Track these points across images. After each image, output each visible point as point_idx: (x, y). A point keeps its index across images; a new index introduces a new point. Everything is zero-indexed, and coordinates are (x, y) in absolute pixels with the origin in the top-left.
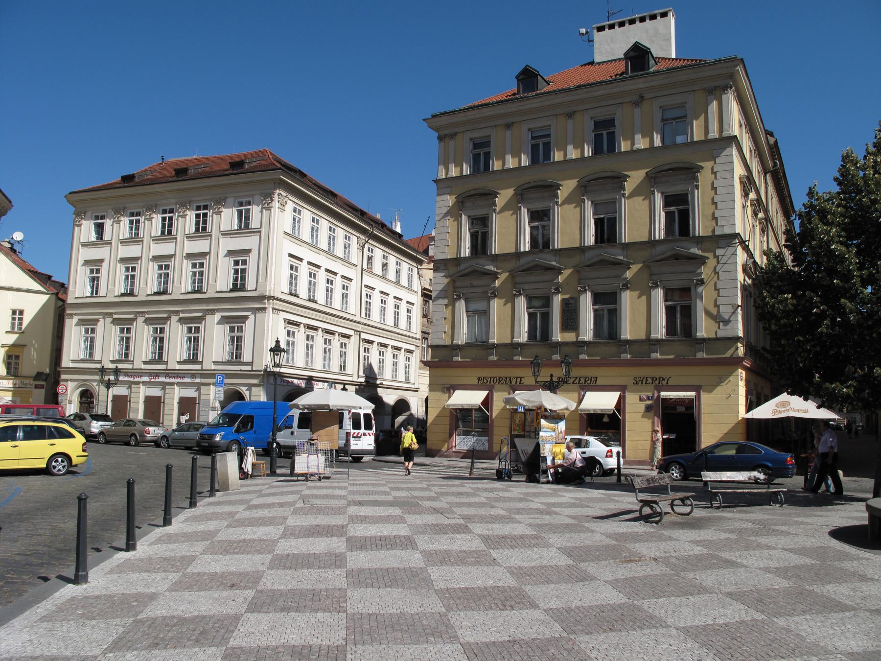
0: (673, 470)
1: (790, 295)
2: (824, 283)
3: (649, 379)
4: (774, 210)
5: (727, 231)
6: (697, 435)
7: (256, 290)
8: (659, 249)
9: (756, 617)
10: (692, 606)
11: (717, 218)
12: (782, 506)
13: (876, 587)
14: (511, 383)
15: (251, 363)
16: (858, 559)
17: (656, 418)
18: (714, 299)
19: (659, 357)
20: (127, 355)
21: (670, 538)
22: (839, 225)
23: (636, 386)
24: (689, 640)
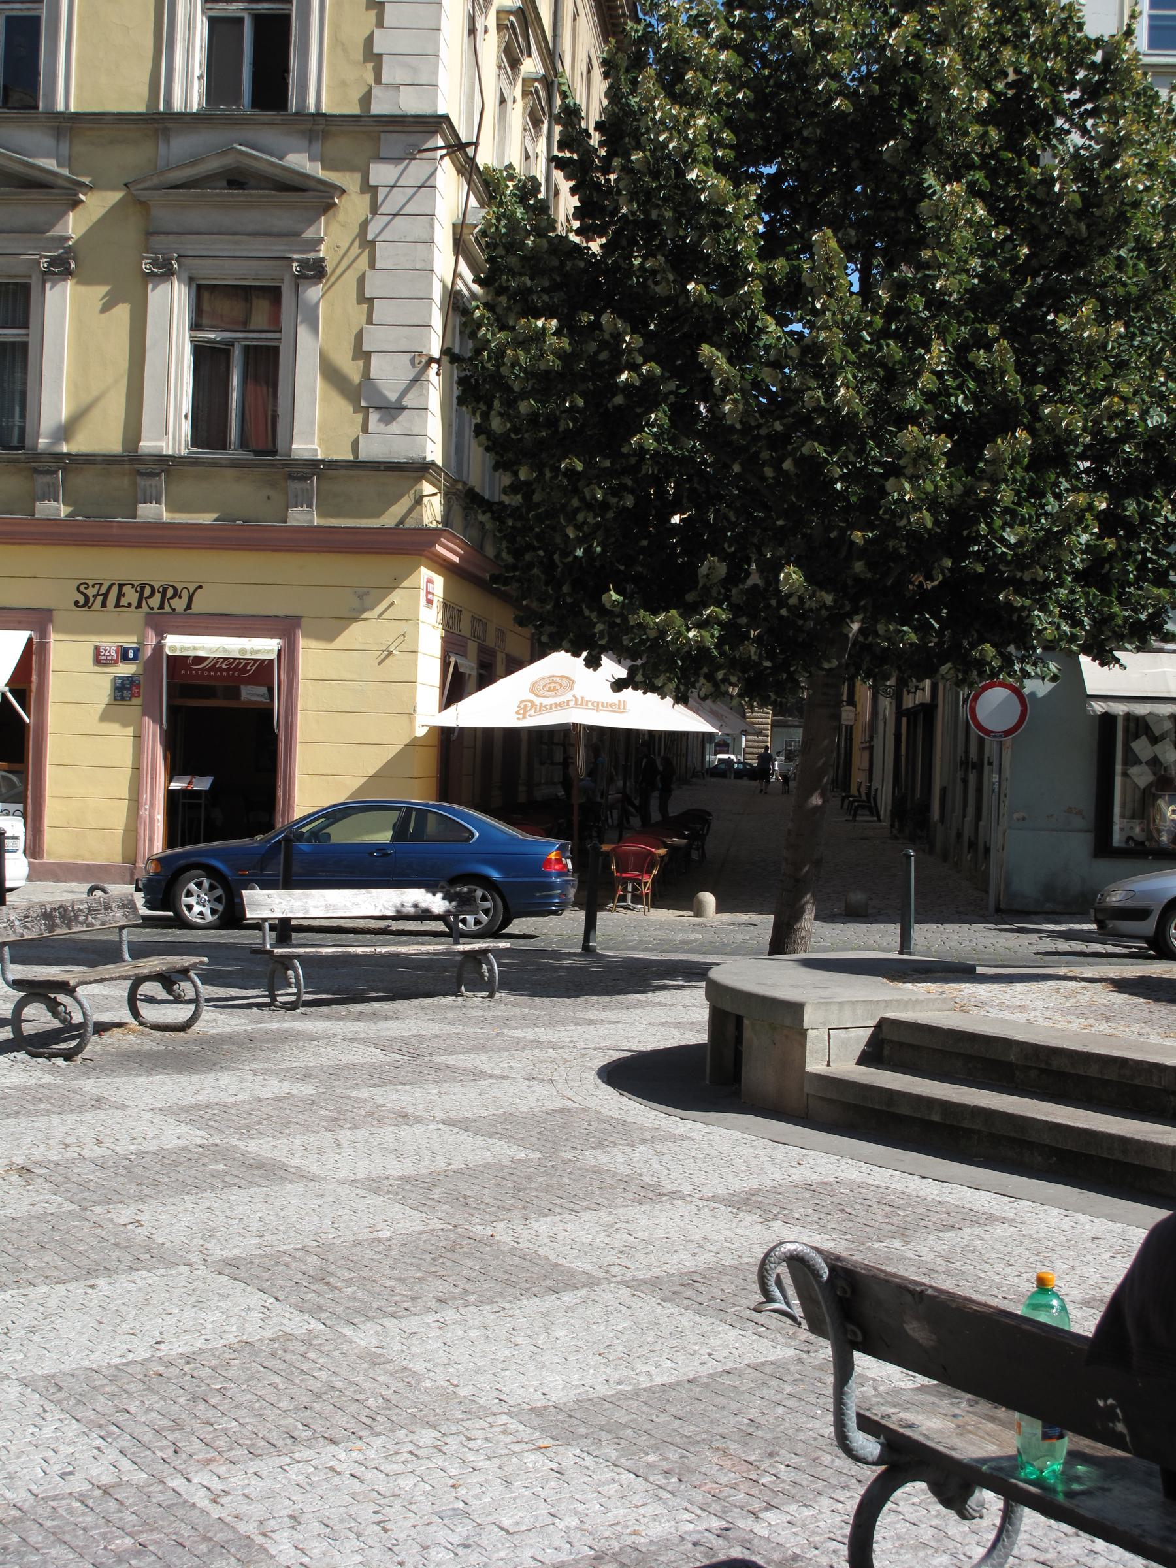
0: (189, 894)
1: (554, 322)
2: (658, 289)
3: (126, 589)
4: (582, 57)
5: (410, 104)
6: (280, 782)
8: (182, 145)
9: (290, 1327)
10: (97, 1310)
11: (380, 55)
12: (491, 996)
13: (676, 1216)
16: (657, 1138)
17: (149, 724)
18: (355, 331)
19: (166, 517)
21: (99, 1102)
22: (717, 105)
23: (83, 614)
24: (55, 1414)
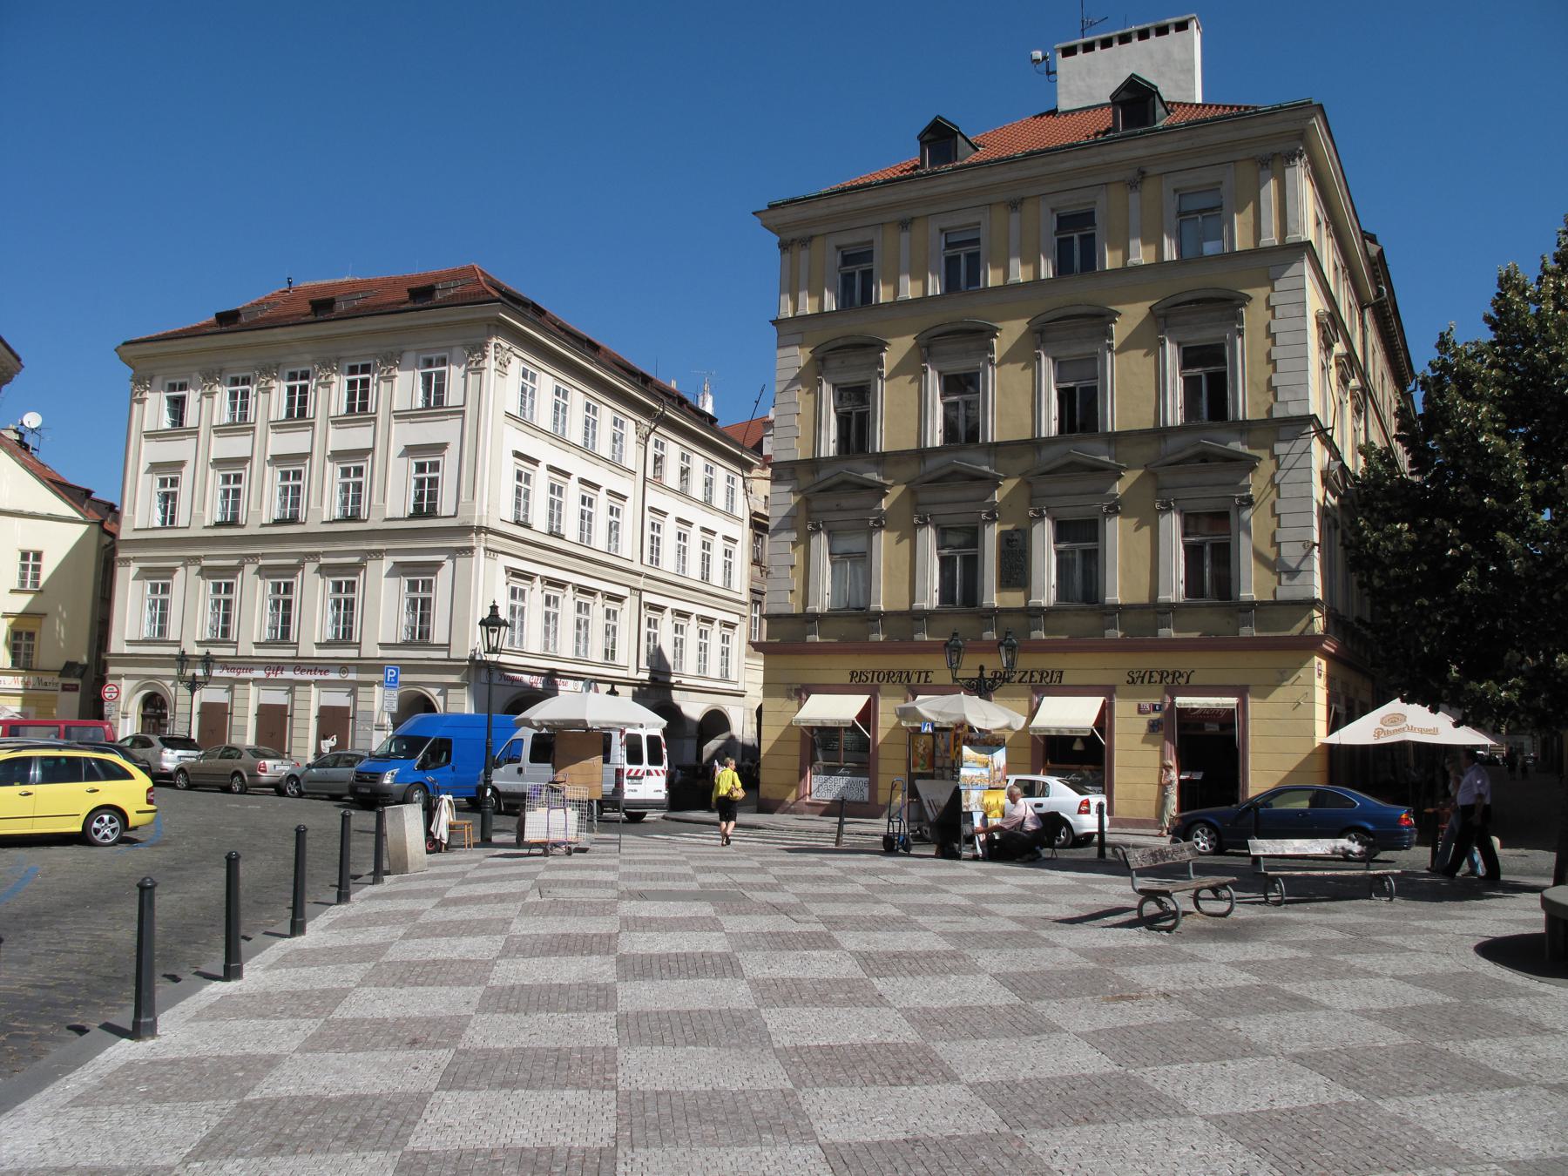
0: (1197, 836)
1: (1406, 525)
2: (1467, 503)
3: (1154, 674)
4: (1378, 373)
5: (1294, 410)
6: (1241, 774)
7: (455, 516)
8: (1173, 443)
9: (1345, 1097)
10: (1231, 1079)
11: (1276, 387)
12: (1391, 900)
13: (1560, 1045)
14: (909, 681)
15: (446, 647)
16: (1528, 994)
17: (1168, 745)
18: (1271, 532)
19: (1173, 635)
20: (225, 632)
21: (1193, 958)
22: (1493, 400)
23: (1131, 687)
24: (1227, 1139)
